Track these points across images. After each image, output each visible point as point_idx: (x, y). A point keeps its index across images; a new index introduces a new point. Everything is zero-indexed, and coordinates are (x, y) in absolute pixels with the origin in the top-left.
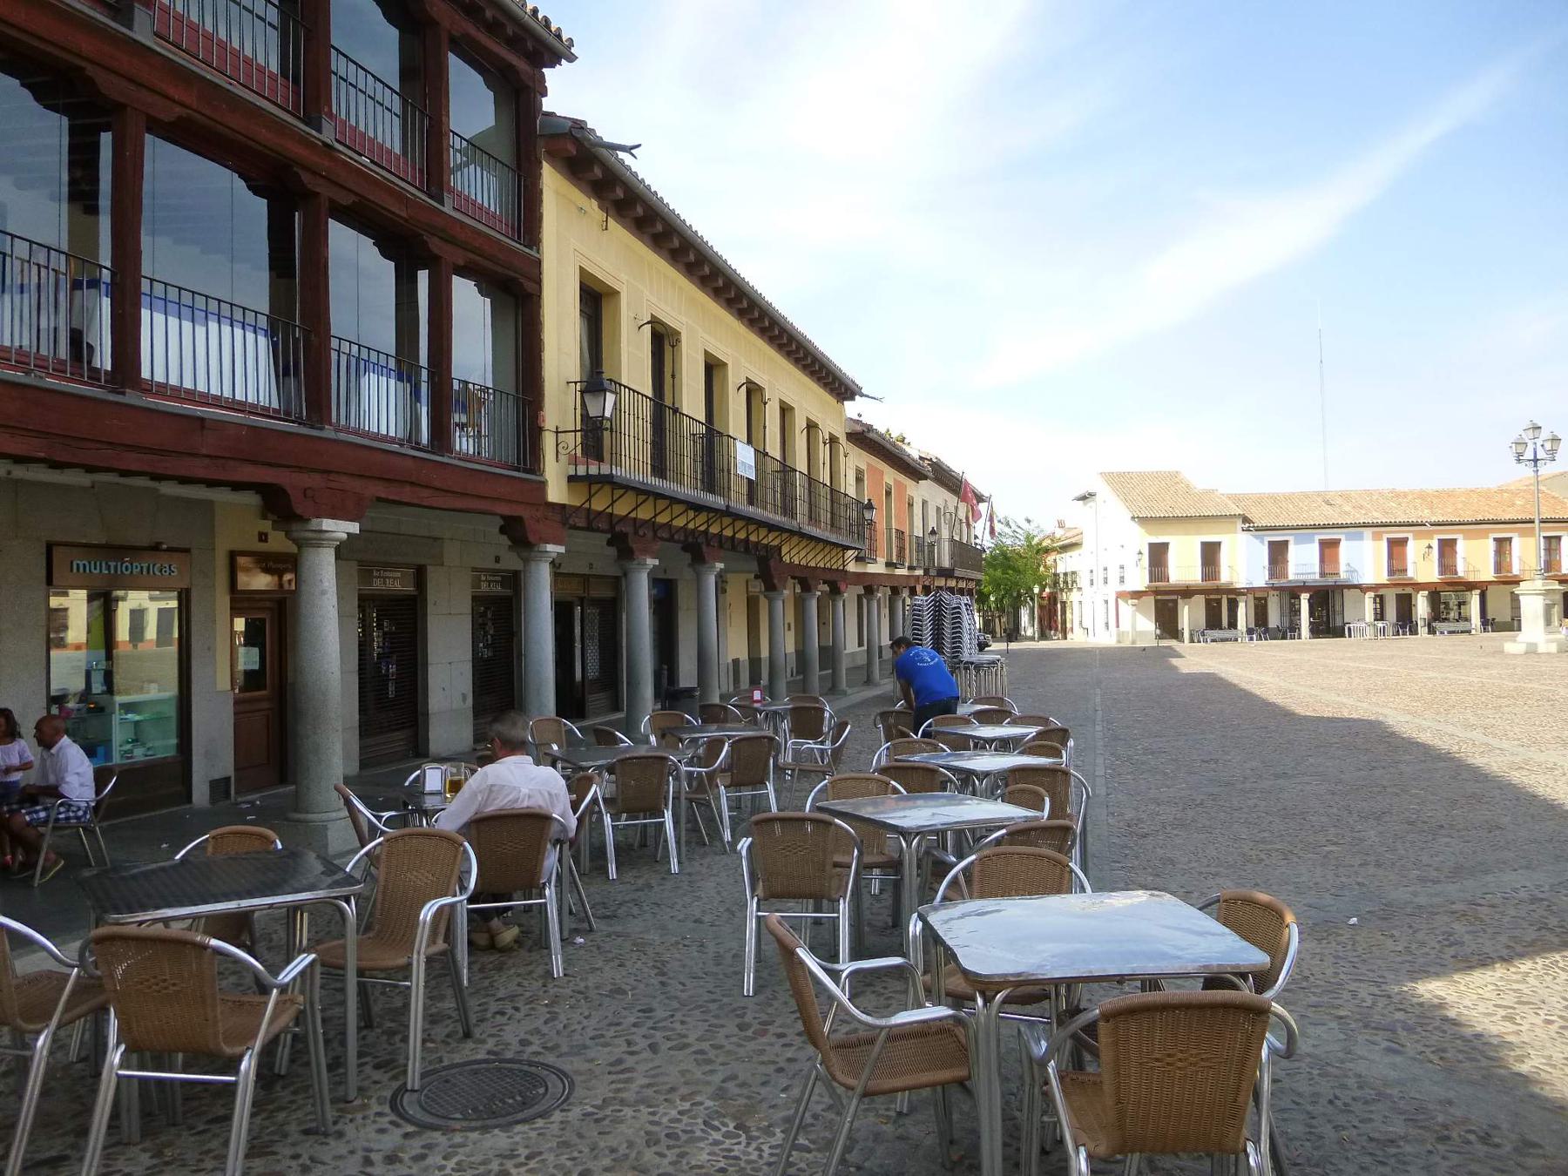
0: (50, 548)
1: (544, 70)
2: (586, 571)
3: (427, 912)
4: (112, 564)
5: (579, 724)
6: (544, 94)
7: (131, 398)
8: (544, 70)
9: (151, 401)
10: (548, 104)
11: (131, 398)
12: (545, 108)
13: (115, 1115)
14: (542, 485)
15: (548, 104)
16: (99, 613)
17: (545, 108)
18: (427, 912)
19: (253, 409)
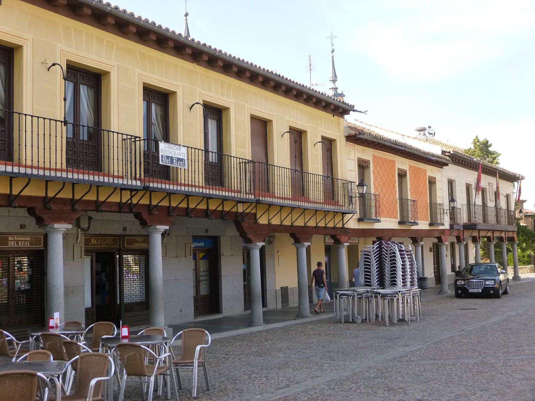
2: (120, 232)
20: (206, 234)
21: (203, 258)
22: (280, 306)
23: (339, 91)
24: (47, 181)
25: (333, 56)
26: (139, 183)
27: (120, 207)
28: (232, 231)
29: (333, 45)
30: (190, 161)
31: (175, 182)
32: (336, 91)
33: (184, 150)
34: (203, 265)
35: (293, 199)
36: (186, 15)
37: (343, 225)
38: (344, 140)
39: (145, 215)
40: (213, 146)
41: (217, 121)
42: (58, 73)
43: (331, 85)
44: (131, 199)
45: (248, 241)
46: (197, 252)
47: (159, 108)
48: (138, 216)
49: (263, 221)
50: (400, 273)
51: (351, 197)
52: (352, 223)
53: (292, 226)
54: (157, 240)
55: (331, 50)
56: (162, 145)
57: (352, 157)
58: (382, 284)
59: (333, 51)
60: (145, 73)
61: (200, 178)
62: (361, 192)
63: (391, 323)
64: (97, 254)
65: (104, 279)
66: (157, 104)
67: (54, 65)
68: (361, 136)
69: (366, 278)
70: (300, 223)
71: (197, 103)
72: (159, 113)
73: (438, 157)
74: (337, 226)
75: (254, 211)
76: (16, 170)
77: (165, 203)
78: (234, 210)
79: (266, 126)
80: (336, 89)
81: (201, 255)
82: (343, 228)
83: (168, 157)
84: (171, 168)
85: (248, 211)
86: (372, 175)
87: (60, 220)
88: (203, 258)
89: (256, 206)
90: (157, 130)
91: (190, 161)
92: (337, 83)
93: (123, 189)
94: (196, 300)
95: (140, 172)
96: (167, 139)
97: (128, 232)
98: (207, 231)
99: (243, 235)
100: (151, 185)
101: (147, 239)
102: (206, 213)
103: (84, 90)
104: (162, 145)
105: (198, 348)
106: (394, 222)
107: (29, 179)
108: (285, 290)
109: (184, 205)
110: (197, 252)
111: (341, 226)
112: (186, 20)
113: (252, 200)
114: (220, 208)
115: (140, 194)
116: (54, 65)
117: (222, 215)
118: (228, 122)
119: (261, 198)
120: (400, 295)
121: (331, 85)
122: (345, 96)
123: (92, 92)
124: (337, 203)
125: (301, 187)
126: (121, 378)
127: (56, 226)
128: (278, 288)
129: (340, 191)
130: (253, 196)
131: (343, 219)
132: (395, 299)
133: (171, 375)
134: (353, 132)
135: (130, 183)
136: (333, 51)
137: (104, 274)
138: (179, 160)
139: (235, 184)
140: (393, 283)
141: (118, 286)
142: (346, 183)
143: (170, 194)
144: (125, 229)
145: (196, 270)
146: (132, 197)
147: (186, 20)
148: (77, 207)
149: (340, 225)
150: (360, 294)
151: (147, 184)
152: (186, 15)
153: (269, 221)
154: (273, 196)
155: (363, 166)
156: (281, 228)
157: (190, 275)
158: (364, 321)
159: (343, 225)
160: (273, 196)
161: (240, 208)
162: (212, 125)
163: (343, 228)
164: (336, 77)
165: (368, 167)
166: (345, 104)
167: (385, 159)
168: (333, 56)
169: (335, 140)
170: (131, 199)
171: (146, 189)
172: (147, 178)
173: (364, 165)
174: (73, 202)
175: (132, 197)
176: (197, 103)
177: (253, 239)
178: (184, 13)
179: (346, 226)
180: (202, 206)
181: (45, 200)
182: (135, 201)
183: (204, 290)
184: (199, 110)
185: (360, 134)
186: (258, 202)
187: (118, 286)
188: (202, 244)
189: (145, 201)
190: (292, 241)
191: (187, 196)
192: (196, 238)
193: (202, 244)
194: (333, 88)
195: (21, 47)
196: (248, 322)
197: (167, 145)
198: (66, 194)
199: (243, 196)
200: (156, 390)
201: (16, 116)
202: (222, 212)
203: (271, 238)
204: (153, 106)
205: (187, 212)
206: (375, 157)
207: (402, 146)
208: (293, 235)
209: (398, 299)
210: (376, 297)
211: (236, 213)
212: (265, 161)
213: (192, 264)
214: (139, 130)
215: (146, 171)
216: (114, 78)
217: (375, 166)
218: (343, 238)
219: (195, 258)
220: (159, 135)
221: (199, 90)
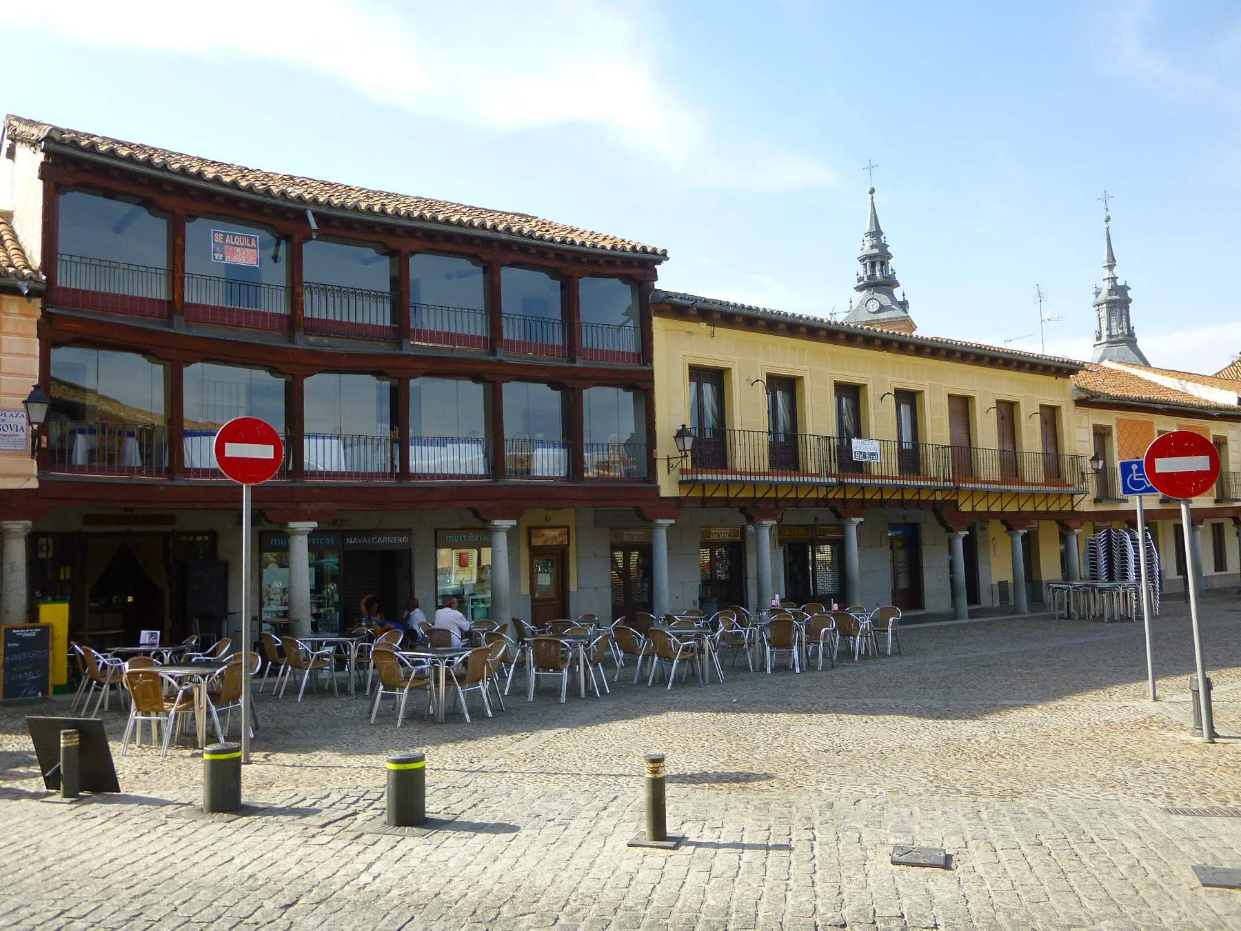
0: (436, 531)
1: (656, 266)
2: (812, 522)
3: (823, 630)
4: (465, 537)
5: (94, 715)
6: (656, 278)
7: (180, 482)
8: (656, 266)
9: (310, 482)
10: (658, 285)
11: (180, 482)
12: (656, 287)
13: (654, 678)
14: (657, 489)
15: (658, 285)
16: (1225, 492)
17: (656, 287)
18: (823, 630)
19: (476, 477)
20: (904, 521)
21: (900, 548)
22: (997, 604)
23: (1120, 282)
24: (754, 485)
25: (1107, 228)
26: (834, 480)
27: (817, 502)
28: (931, 517)
29: (1107, 210)
30: (882, 454)
31: (868, 475)
32: (1115, 282)
33: (876, 444)
34: (902, 555)
35: (1003, 482)
36: (872, 191)
37: (1073, 507)
38: (1072, 405)
39: (840, 508)
40: (907, 436)
41: (910, 405)
42: (761, 388)
43: (1107, 274)
44: (827, 495)
45: (949, 530)
46: (894, 541)
47: (849, 402)
48: (833, 510)
49: (966, 508)
50: (1132, 565)
51: (1083, 474)
52: (1085, 505)
53: (1002, 512)
54: (853, 532)
55: (1104, 218)
56: (855, 441)
57: (1085, 425)
58: (1111, 577)
59: (1108, 220)
60: (836, 372)
61: (893, 469)
62: (1095, 467)
63: (1111, 620)
64: (789, 544)
65: (796, 570)
66: (847, 398)
67: (757, 381)
68: (1094, 400)
69: (1091, 571)
70: (1012, 508)
71: (888, 393)
72: (849, 406)
73: (1234, 410)
74: (1064, 509)
75: (954, 498)
76: (729, 477)
77: (859, 496)
78: (932, 498)
79: (967, 405)
80: (1114, 279)
81: (899, 544)
82: (1073, 511)
83: (861, 453)
84: (864, 464)
85: (947, 498)
86: (1115, 444)
87: (766, 517)
88: (900, 548)
89: (957, 493)
90: (848, 423)
91: (882, 454)
92: (1115, 270)
93: (818, 486)
94: (894, 594)
95: (835, 468)
96: (859, 436)
97: (820, 522)
98: (904, 518)
99: (942, 523)
100: (846, 481)
101: (842, 529)
102: (901, 503)
103: (779, 394)
104: (855, 441)
105: (891, 619)
106: (1152, 501)
107: (743, 484)
108: (1003, 585)
109: (878, 497)
110: (894, 541)
111: (1070, 509)
112: (872, 199)
113: (950, 487)
114: (916, 497)
115: (836, 489)
116: (757, 381)
117: (918, 504)
118: (923, 406)
119: (961, 485)
120: (1121, 589)
121: (1107, 274)
122: (1130, 289)
123: (786, 396)
124: (1063, 484)
125: (1014, 469)
126: (835, 640)
127: (764, 522)
128: (995, 582)
129: (1067, 467)
130: (952, 484)
131: (1072, 500)
132: (1115, 593)
133: (871, 637)
134: (1083, 395)
135: (826, 481)
136: (1108, 220)
137: (796, 565)
138: (874, 454)
139: (932, 472)
140: (1124, 576)
141: (811, 577)
142: (1075, 458)
143: (863, 488)
144: (816, 519)
145: (893, 560)
146: (827, 493)
147: (872, 199)
148: (780, 505)
149: (1068, 508)
150: (1077, 588)
151: (842, 480)
152: (872, 191)
153: (973, 508)
154: (977, 481)
155: (1101, 434)
156: (989, 515)
157: (888, 567)
158: (1082, 618)
159: (1073, 507)
160: (977, 481)
161: (939, 497)
162: (905, 409)
163: (1073, 511)
164: (1114, 260)
165: (1110, 434)
166: (1071, 363)
167: (1136, 422)
168: (1107, 228)
169: (1059, 407)
170: (827, 495)
171: (841, 485)
172: (841, 474)
173: (1102, 432)
174: (776, 500)
175: (827, 493)
176: (888, 393)
177: (955, 528)
178: (869, 190)
179: (1076, 509)
180: (898, 497)
181: (754, 500)
182: (830, 496)
183: (903, 584)
184: (891, 400)
185: (1093, 397)
186: (958, 489)
187: (811, 577)
188: (899, 532)
189: (840, 495)
190: (1004, 528)
191: (881, 488)
192: (892, 526)
193: (899, 532)
194: (1109, 279)
195: (729, 369)
196: (954, 616)
197: (860, 441)
198: (772, 495)
199: (941, 484)
200: (860, 652)
201: (728, 432)
202: (919, 500)
203: (984, 524)
204: (844, 400)
205: (881, 503)
206: (1119, 421)
207: (1162, 404)
208: (1004, 522)
209: (1118, 594)
210: (1093, 591)
211: (935, 501)
212: (968, 446)
213: (889, 553)
214: (831, 429)
215: (841, 466)
216: (807, 382)
217: (1120, 432)
218: (1072, 524)
219: (892, 547)
220: (851, 430)
221: (890, 378)
